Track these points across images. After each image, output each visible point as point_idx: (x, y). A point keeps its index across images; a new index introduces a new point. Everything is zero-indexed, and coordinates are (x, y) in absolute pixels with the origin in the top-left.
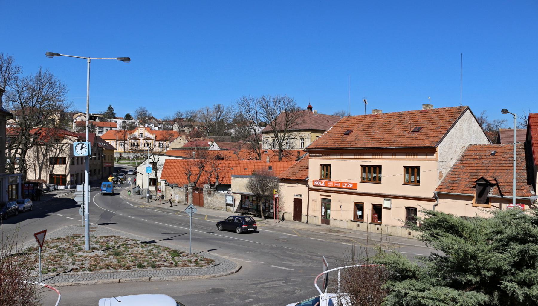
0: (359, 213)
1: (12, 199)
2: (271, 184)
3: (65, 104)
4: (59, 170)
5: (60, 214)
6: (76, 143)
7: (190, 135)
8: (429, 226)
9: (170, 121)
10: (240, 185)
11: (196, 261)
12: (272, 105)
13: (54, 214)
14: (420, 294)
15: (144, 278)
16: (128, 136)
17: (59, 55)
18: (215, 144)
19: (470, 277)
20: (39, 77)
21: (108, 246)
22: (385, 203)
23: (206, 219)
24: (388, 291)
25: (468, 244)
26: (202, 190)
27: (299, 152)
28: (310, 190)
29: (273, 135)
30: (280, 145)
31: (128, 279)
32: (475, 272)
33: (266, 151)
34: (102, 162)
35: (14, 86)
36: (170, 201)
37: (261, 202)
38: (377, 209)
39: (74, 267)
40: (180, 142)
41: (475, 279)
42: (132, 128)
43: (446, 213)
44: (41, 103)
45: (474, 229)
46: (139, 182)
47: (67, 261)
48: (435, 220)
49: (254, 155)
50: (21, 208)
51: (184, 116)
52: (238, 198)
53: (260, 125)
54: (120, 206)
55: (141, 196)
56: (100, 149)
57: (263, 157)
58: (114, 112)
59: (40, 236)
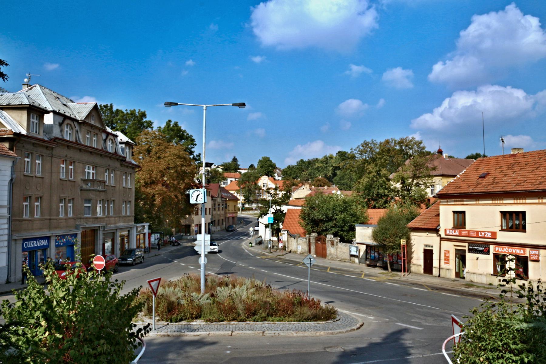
23: (328, 271)
28: (442, 239)
34: (226, 213)
52: (363, 248)
58: (239, 163)
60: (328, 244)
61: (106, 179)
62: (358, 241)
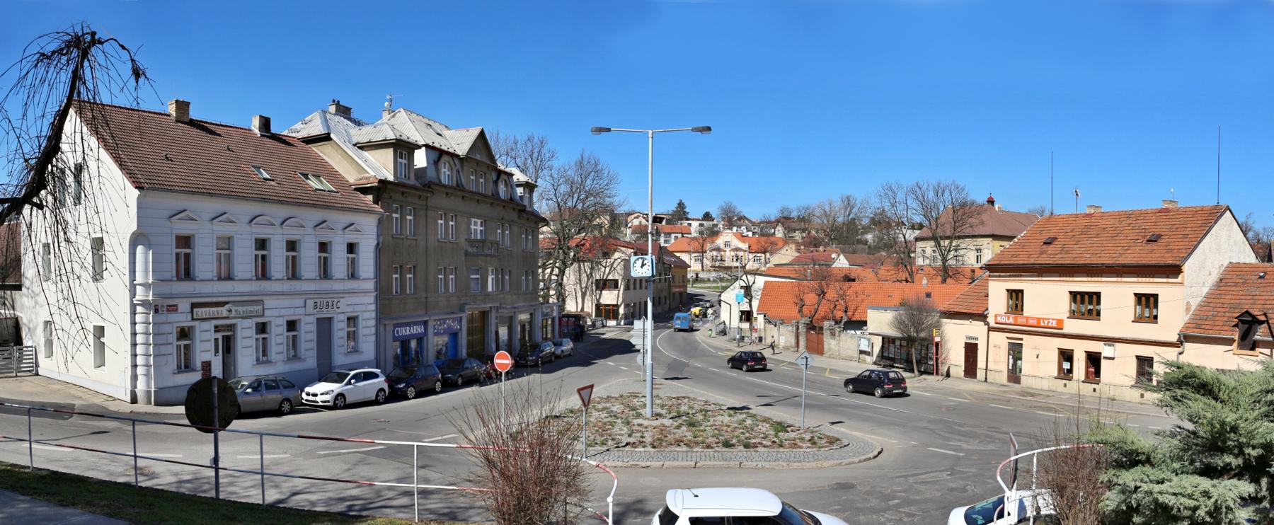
0: (1066, 366)
1: (546, 339)
2: (930, 321)
3: (616, 200)
4: (609, 297)
5: (610, 362)
6: (633, 258)
7: (803, 244)
8: (1171, 384)
9: (769, 222)
10: (881, 322)
11: (811, 440)
12: (931, 195)
13: (601, 362)
14: (1157, 488)
15: (732, 463)
16: (708, 246)
17: (609, 130)
18: (842, 257)
19: (1228, 459)
20: (580, 164)
21: (678, 412)
22: (1106, 350)
23: (827, 374)
24: (1110, 485)
25: (1227, 409)
26: (821, 328)
27: (973, 271)
28: (990, 329)
29: (932, 243)
30: (944, 260)
31: (708, 463)
32: (1236, 451)
33: (921, 268)
35: (548, 178)
36: (772, 346)
37: (912, 351)
38: (1094, 360)
39: (631, 440)
40: (787, 255)
41: (1235, 462)
42: (714, 233)
43: (1196, 364)
44: (584, 201)
45: (1235, 388)
46: (724, 316)
47: (620, 430)
48: (1179, 374)
49: (904, 275)
50: (558, 352)
51: (794, 214)
52: (878, 342)
53: (913, 228)
54: (694, 350)
55: (727, 337)
56: (668, 266)
57: (916, 277)
59: (585, 392)
60: (826, 334)
61: (499, 238)
62: (870, 331)
